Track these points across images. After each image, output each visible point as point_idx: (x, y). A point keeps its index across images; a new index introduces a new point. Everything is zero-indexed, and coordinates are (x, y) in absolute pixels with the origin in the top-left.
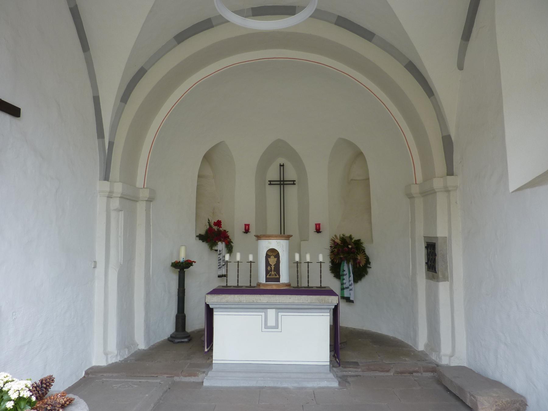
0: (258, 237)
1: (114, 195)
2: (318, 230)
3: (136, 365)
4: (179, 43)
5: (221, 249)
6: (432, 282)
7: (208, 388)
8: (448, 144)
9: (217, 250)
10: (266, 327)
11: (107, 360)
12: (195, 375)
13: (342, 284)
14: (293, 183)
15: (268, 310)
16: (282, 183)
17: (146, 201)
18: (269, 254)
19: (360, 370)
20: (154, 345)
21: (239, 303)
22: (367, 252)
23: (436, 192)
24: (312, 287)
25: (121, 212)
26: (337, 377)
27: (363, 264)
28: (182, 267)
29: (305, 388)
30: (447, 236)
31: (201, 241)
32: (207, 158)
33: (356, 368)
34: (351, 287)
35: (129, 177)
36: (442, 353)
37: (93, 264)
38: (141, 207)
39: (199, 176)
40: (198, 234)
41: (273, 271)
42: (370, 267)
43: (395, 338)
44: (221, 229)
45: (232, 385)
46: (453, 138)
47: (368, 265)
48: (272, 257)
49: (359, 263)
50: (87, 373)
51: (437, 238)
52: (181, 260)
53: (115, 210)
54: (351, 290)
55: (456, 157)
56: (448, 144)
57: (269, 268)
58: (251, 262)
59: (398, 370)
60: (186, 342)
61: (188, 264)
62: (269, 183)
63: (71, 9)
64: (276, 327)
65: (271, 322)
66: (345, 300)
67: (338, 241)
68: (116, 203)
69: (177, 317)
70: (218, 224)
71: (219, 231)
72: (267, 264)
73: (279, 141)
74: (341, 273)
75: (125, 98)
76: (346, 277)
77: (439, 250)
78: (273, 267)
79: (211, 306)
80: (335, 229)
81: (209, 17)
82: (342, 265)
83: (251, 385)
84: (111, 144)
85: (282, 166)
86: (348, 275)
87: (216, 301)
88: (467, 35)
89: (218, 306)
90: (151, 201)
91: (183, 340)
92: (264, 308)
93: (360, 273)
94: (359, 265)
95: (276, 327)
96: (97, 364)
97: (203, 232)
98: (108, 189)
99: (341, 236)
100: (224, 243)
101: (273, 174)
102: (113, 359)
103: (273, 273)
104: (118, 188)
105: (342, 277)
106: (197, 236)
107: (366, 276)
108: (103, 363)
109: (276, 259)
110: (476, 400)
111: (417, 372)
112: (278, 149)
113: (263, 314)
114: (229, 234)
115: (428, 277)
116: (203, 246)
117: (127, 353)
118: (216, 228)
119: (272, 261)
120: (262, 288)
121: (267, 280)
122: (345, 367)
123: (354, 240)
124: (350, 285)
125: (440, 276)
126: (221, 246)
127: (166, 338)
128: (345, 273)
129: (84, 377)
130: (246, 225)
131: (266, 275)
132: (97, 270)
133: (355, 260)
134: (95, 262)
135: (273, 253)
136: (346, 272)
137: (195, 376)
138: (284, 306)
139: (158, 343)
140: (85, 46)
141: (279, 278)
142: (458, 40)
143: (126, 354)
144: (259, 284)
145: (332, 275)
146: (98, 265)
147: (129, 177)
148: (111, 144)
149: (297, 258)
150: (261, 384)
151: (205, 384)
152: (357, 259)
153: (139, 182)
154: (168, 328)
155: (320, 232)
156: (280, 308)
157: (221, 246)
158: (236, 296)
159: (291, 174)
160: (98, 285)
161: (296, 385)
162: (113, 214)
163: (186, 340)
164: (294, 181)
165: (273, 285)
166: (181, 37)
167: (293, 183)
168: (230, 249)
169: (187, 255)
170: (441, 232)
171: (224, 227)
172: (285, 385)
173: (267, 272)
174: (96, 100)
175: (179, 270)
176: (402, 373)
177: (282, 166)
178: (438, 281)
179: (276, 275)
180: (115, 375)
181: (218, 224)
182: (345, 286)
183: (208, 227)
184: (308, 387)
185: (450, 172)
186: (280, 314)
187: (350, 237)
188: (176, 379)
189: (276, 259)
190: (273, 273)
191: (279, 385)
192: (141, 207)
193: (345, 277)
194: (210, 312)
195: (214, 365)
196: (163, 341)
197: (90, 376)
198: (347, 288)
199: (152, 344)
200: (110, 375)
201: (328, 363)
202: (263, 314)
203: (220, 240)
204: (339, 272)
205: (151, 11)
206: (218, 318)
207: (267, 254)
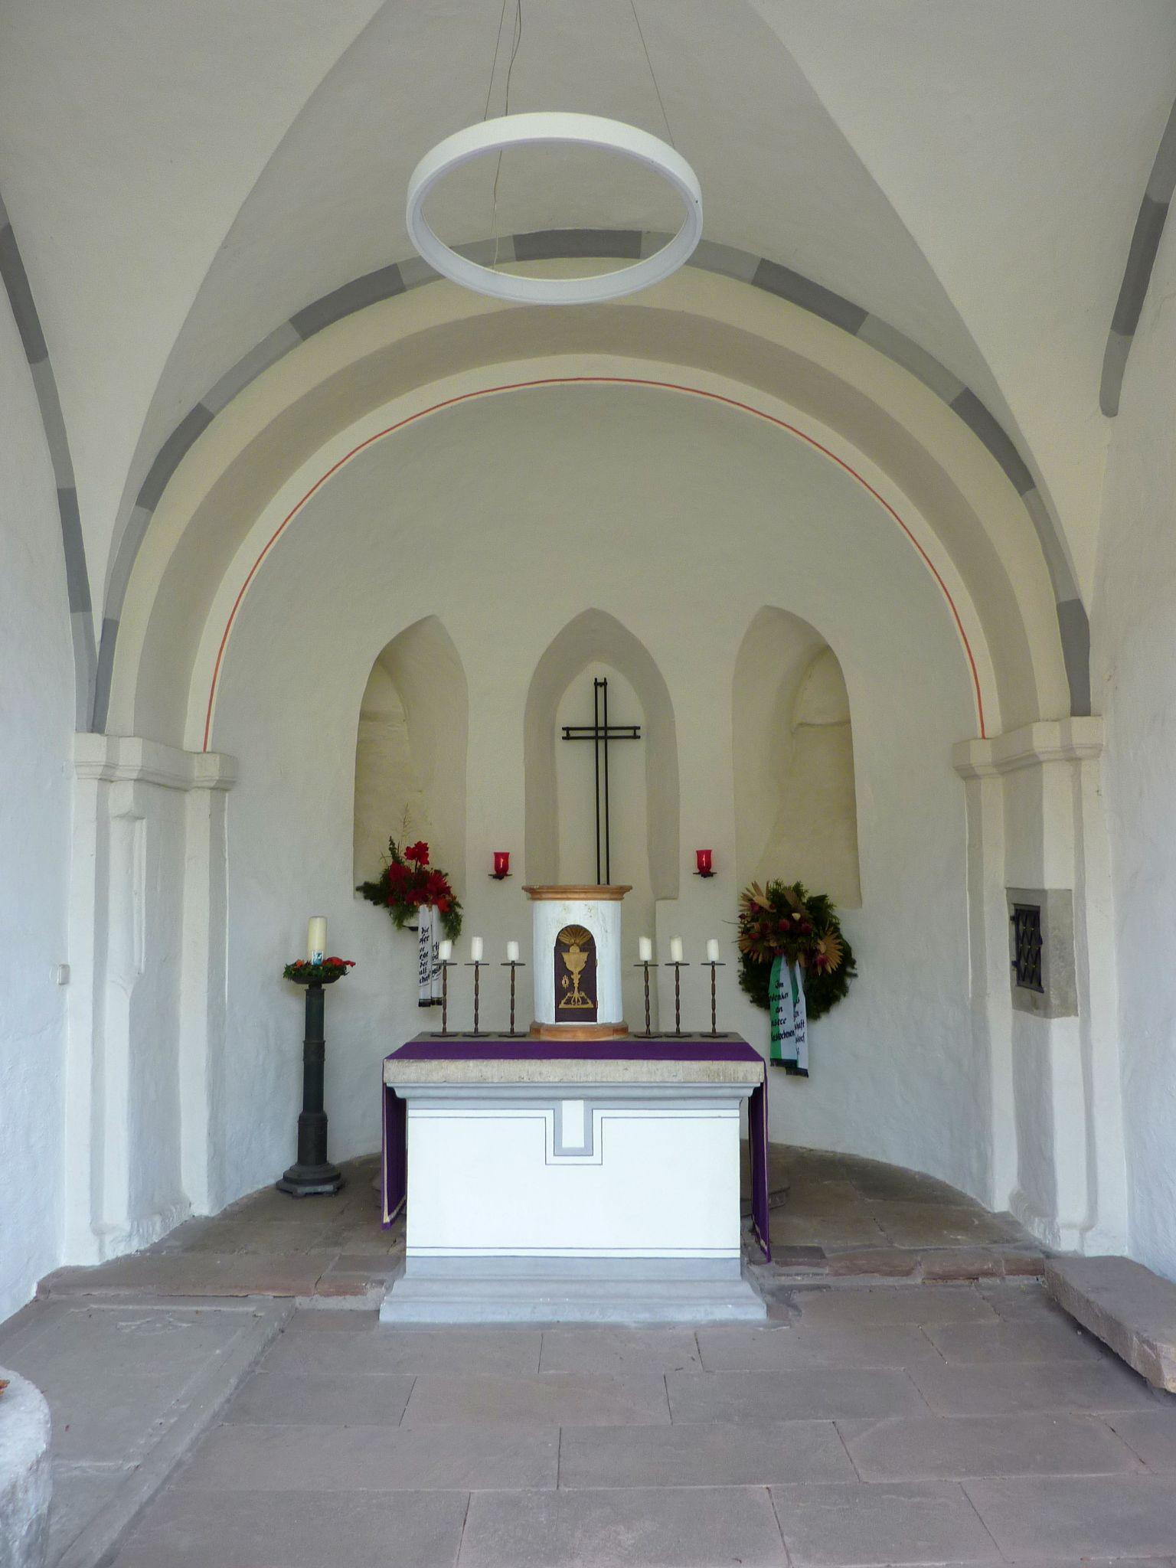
0: (535, 893)
1: (118, 773)
2: (705, 869)
3: (184, 1263)
4: (757, 282)
5: (427, 925)
6: (1031, 1019)
7: (393, 1327)
8: (1073, 623)
9: (414, 929)
10: (559, 1151)
12: (356, 1291)
13: (775, 1023)
15: (565, 1103)
16: (601, 734)
17: (212, 789)
18: (566, 940)
19: (827, 1270)
20: (236, 1204)
21: (481, 1083)
22: (848, 931)
23: (1040, 763)
24: (689, 1035)
25: (138, 824)
26: (762, 1291)
29: (673, 1325)
30: (1072, 886)
31: (369, 903)
32: (387, 663)
33: (817, 1265)
34: (799, 1033)
35: (160, 719)
37: (59, 972)
38: (196, 807)
39: (364, 716)
40: (361, 884)
41: (577, 990)
42: (855, 975)
44: (427, 867)
45: (462, 1319)
47: (849, 970)
48: (574, 949)
49: (823, 962)
50: (42, 1288)
51: (1042, 893)
52: (314, 959)
53: (122, 817)
54: (800, 1039)
55: (1098, 663)
56: (1073, 623)
57: (565, 982)
58: (513, 964)
59: (937, 1269)
60: (329, 1194)
61: (334, 969)
62: (564, 734)
64: (588, 1150)
65: (573, 1138)
66: (783, 1070)
67: (763, 901)
68: (123, 797)
69: (303, 1122)
70: (419, 852)
71: (422, 874)
72: (561, 969)
73: (592, 614)
74: (772, 992)
75: (149, 493)
76: (786, 1004)
77: (1050, 926)
78: (576, 978)
79: (399, 1094)
80: (754, 864)
83: (517, 1319)
84: (110, 627)
85: (601, 685)
87: (413, 1077)
88: (1127, 317)
89: (419, 1093)
90: (226, 790)
91: (320, 1189)
92: (551, 1097)
93: (826, 990)
94: (824, 970)
95: (588, 1150)
96: (74, 1263)
97: (375, 877)
98: (101, 757)
99: (772, 885)
100: (435, 908)
101: (576, 709)
102: (118, 1249)
103: (576, 995)
104: (132, 754)
105: (773, 1004)
106: (358, 889)
109: (584, 956)
110: (1158, 1356)
112: (592, 636)
113: (549, 1114)
114: (450, 881)
115: (1019, 1004)
116: (378, 916)
118: (411, 865)
119: (575, 960)
120: (545, 1037)
121: (560, 1015)
122: (786, 1264)
124: (798, 1026)
125: (1054, 1001)
126: (427, 916)
127: (272, 1181)
128: (782, 991)
129: (36, 1300)
130: (498, 856)
132: (70, 992)
133: (811, 954)
134: (65, 967)
135: (576, 938)
137: (354, 1294)
138: (648, 1093)
139: (249, 1197)
140: (35, 348)
143: (156, 1232)
144: (537, 1028)
147: (160, 719)
148: (110, 627)
150: (544, 1314)
151: (384, 1317)
152: (817, 951)
153: (192, 735)
154: (276, 1155)
156: (596, 1097)
157: (427, 916)
158: (471, 1063)
160: (75, 1035)
161: (644, 1316)
162: (117, 829)
163: (329, 1188)
165: (577, 1031)
166: (312, 320)
168: (452, 924)
169: (328, 942)
170: (1054, 876)
171: (434, 864)
172: (613, 1317)
174: (67, 502)
175: (307, 987)
176: (945, 1277)
177: (601, 685)
179: (584, 1002)
180: (124, 1292)
181: (419, 852)
182: (782, 1029)
183: (390, 861)
185: (1081, 707)
187: (798, 890)
188: (301, 1302)
189: (584, 956)
190: (576, 995)
191: (595, 1317)
192: (196, 807)
193: (782, 1003)
194: (395, 1110)
197: (54, 1296)
198: (790, 1034)
199: (230, 1199)
200: (112, 1292)
202: (549, 1114)
203: (425, 900)
204: (766, 989)
205: (224, 246)
206: (420, 1126)
207: (558, 942)
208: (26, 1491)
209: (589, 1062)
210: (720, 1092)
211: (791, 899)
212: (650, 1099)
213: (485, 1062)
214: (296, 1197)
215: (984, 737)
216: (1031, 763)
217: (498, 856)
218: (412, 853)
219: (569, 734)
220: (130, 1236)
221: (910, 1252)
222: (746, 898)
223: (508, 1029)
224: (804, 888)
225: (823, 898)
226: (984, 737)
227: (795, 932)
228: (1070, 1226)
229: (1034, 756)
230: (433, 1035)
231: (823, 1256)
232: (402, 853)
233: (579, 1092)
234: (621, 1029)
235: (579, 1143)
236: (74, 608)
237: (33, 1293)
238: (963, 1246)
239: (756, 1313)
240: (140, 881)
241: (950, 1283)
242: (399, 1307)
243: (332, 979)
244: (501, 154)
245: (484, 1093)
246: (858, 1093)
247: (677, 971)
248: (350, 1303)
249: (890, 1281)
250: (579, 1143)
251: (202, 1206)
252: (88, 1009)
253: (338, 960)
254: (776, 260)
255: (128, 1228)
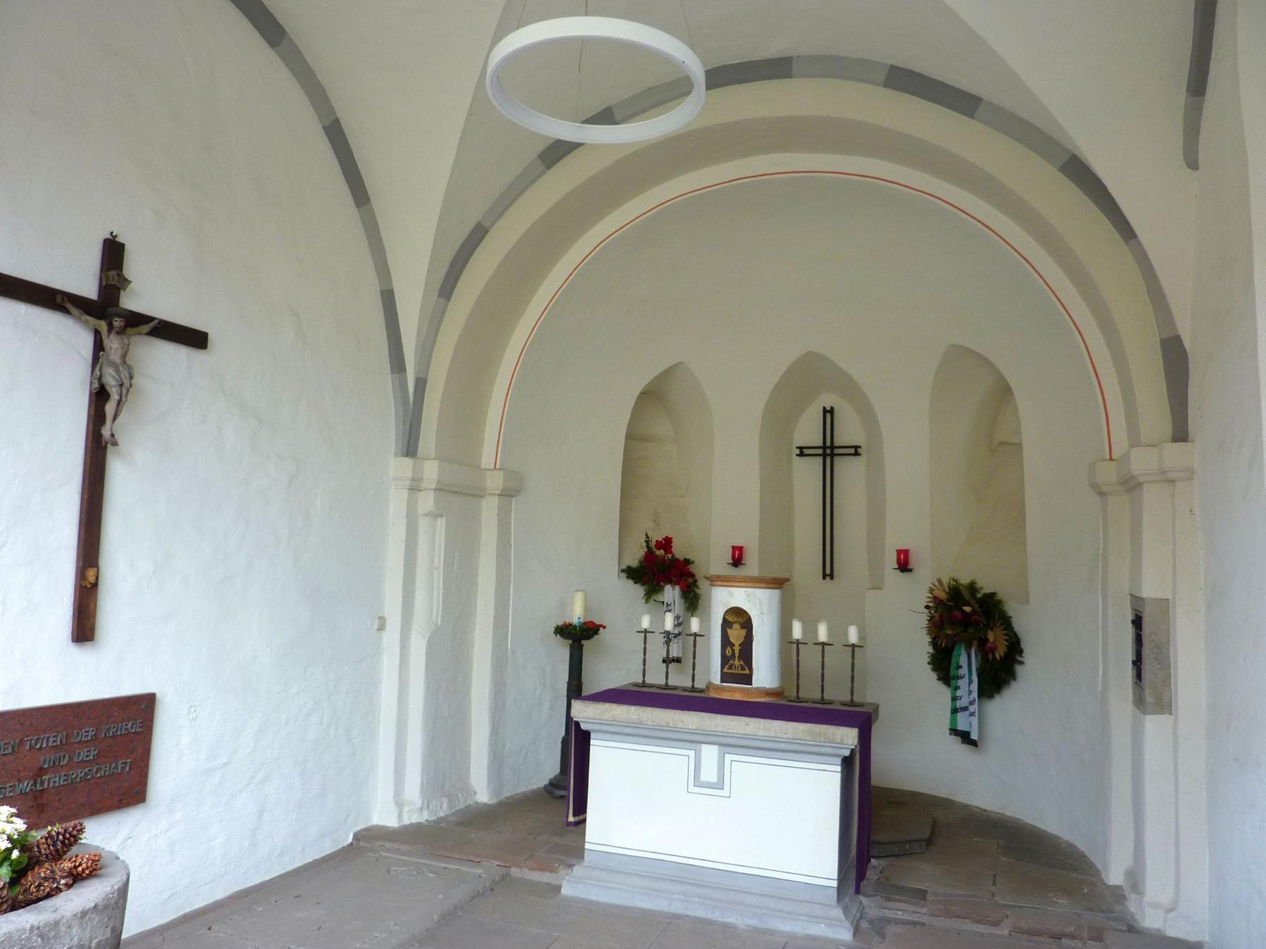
2: (904, 564)
3: (453, 834)
4: (549, 166)
7: (568, 899)
10: (698, 783)
11: (400, 816)
13: (954, 699)
14: (856, 451)
16: (829, 452)
18: (730, 619)
19: (924, 910)
21: (639, 725)
22: (1019, 625)
23: (1141, 484)
24: (831, 703)
25: (439, 520)
27: (1001, 652)
28: (578, 636)
29: (772, 932)
31: (631, 582)
32: (653, 396)
33: (916, 904)
34: (972, 709)
36: (1147, 899)
37: (377, 622)
38: (489, 508)
40: (624, 567)
41: (738, 659)
42: (1022, 663)
43: (1070, 845)
45: (619, 902)
46: (1187, 344)
48: (736, 626)
49: (993, 650)
50: (357, 837)
52: (575, 621)
53: (427, 515)
54: (972, 714)
57: (729, 652)
63: (327, 130)
64: (719, 785)
65: (709, 774)
66: (959, 739)
67: (942, 595)
68: (427, 501)
70: (666, 544)
71: (675, 561)
72: (726, 641)
73: (810, 357)
74: (952, 672)
75: (447, 289)
76: (963, 683)
78: (737, 649)
79: (583, 727)
81: (607, 105)
82: (955, 653)
84: (421, 384)
86: (966, 679)
87: (591, 715)
90: (512, 496)
92: (693, 740)
93: (998, 674)
95: (719, 785)
96: (382, 823)
97: (633, 560)
98: (409, 474)
100: (677, 588)
101: (809, 432)
102: (414, 816)
105: (953, 682)
107: (1013, 683)
108: (392, 822)
109: (744, 632)
111: (1072, 937)
112: (809, 374)
113: (692, 753)
116: (638, 591)
117: (445, 806)
119: (736, 635)
121: (725, 678)
122: (889, 899)
123: (983, 592)
124: (971, 703)
126: (671, 593)
130: (734, 548)
131: (722, 668)
133: (983, 642)
134: (382, 619)
135: (738, 618)
136: (964, 671)
137: (551, 872)
138: (734, 741)
141: (751, 676)
142: (1180, 96)
143: (443, 809)
145: (934, 676)
146: (388, 626)
148: (421, 384)
149: (797, 631)
150: (678, 908)
151: (564, 891)
152: (987, 640)
155: (910, 570)
156: (729, 744)
157: (671, 593)
158: (633, 708)
159: (848, 432)
161: (753, 922)
162: (423, 524)
164: (856, 447)
165: (735, 692)
167: (856, 451)
169: (587, 609)
170: (1149, 591)
171: (679, 551)
172: (730, 919)
173: (725, 660)
176: (1031, 933)
177: (829, 412)
178: (1145, 713)
179: (743, 669)
180: (404, 847)
181: (666, 544)
182: (959, 704)
184: (780, 932)
185: (1180, 435)
186: (728, 758)
188: (515, 872)
189: (744, 632)
190: (737, 662)
191: (715, 916)
192: (489, 508)
193: (960, 683)
195: (586, 853)
196: (534, 791)
197: (362, 843)
198: (965, 709)
199: (507, 793)
200: (396, 847)
201: (835, 884)
202: (692, 753)
203: (670, 582)
204: (948, 669)
206: (598, 750)
207: (725, 620)
208: (70, 927)
209: (719, 716)
210: (823, 750)
211: (967, 595)
212: (776, 750)
213: (643, 708)
214: (555, 797)
215: (1111, 459)
216: (1131, 485)
217: (734, 548)
218: (659, 545)
219: (802, 452)
220: (421, 809)
221: (1006, 906)
222: (931, 591)
223: (690, 685)
224: (979, 585)
225: (993, 595)
226: (1111, 459)
227: (966, 622)
228: (1155, 905)
229: (1133, 478)
230: (636, 685)
231: (925, 899)
232: (653, 544)
233: (713, 739)
234: (769, 693)
235: (714, 779)
236: (393, 371)
237: (350, 840)
238: (1059, 909)
239: (844, 934)
240: (439, 561)
241: (1034, 938)
242: (575, 885)
243: (589, 637)
244: (583, 43)
245: (643, 732)
246: (1006, 766)
247: (853, 652)
248: (546, 877)
249: (981, 928)
250: (714, 779)
251: (483, 796)
252: (397, 650)
253: (592, 622)
254: (901, 65)
255: (420, 804)
